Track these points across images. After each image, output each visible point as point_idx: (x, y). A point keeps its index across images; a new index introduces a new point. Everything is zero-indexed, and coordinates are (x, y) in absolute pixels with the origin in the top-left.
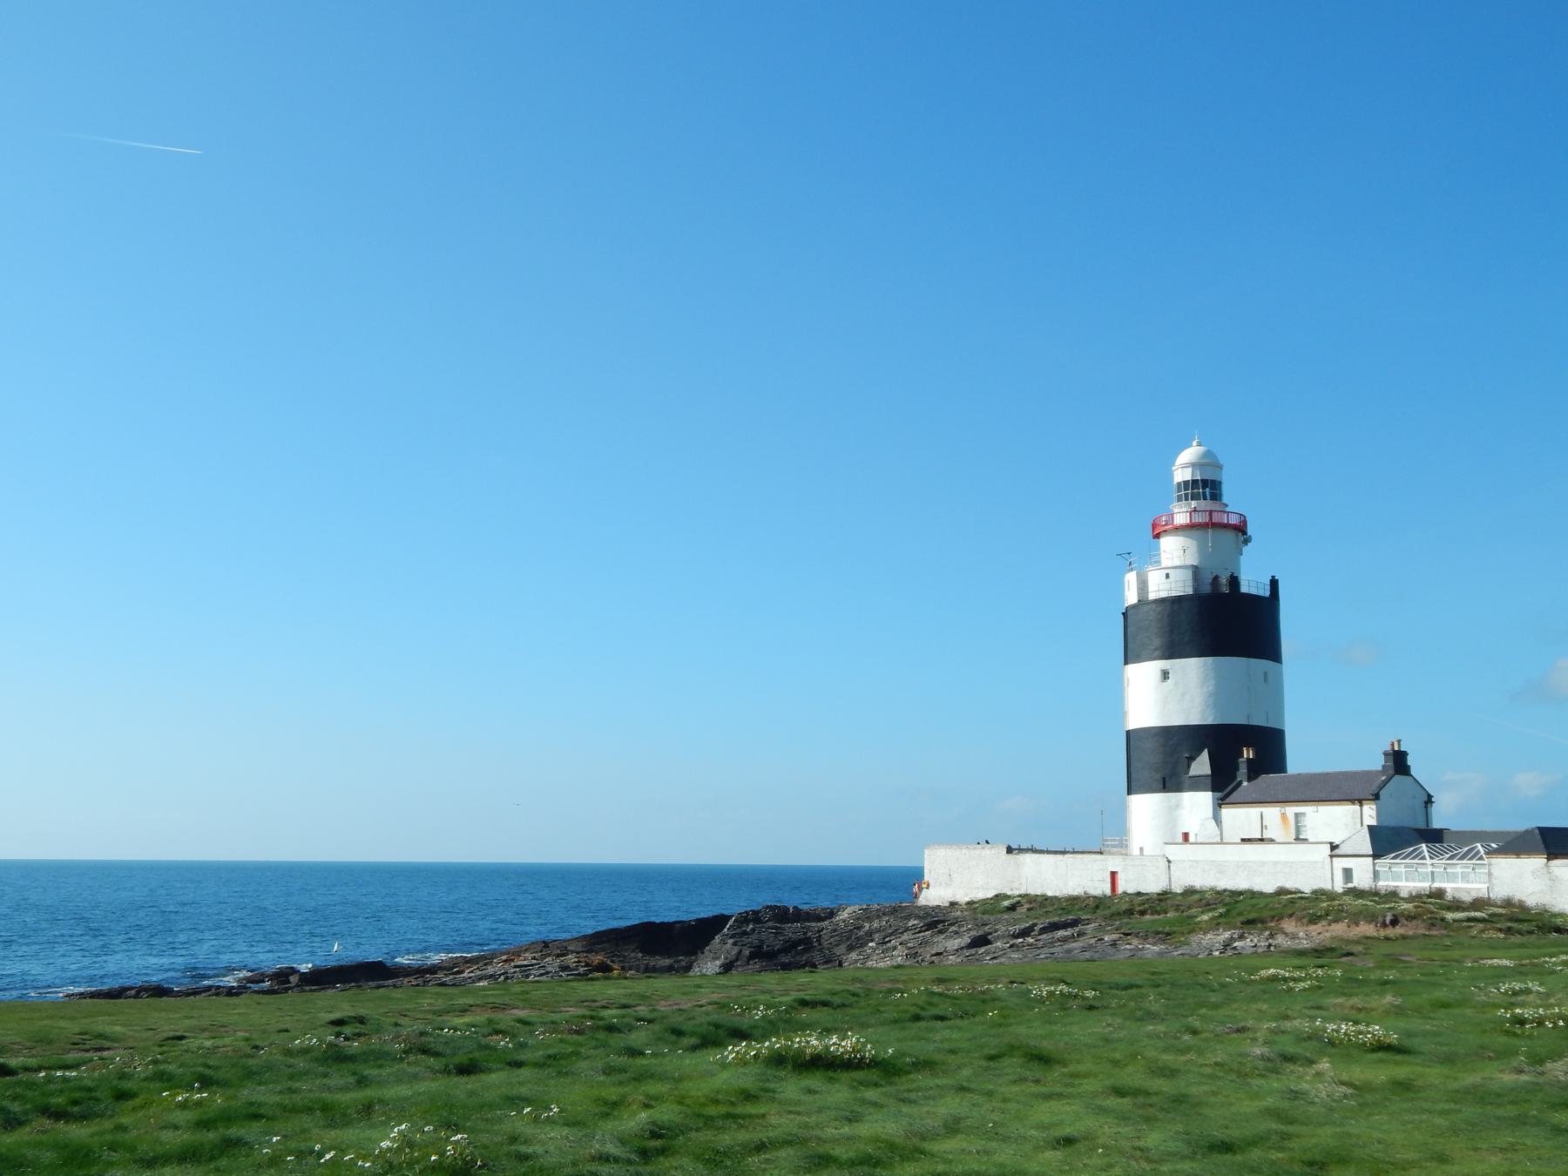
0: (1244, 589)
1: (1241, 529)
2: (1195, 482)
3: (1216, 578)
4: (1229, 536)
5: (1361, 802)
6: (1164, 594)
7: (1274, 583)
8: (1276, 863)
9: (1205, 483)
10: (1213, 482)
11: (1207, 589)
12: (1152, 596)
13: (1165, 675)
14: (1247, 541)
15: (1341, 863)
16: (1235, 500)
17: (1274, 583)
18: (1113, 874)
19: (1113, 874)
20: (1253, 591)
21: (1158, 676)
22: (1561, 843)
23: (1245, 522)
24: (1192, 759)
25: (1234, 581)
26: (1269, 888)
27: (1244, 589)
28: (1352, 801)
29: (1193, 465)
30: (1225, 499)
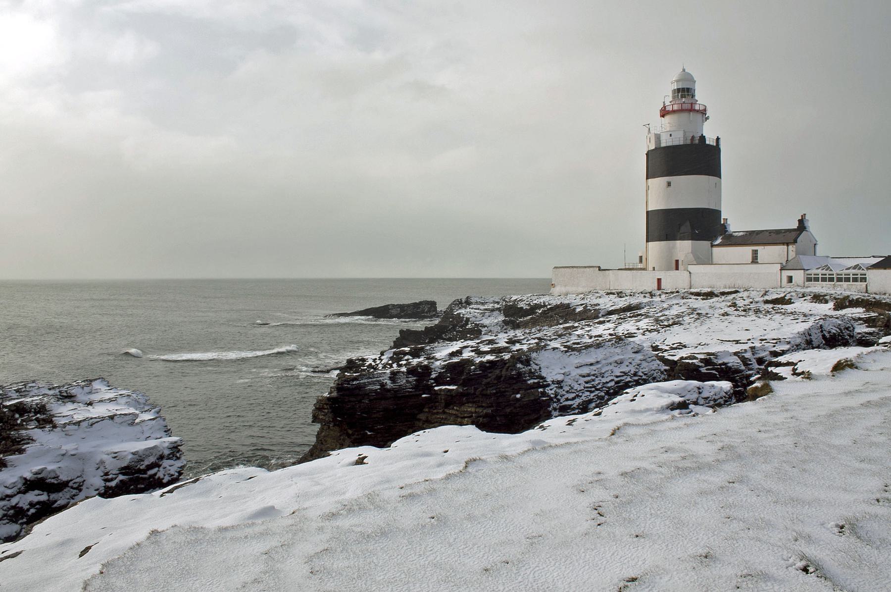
0: (707, 142)
1: (703, 112)
2: (678, 90)
3: (693, 137)
4: (700, 116)
5: (788, 244)
6: (670, 144)
7: (718, 139)
8: (283, 466)
9: (683, 90)
10: (688, 90)
11: (689, 142)
12: (663, 145)
13: (669, 184)
14: (707, 118)
15: (786, 273)
16: (701, 97)
17: (718, 139)
18: (659, 280)
19: (659, 280)
20: (711, 143)
21: (666, 184)
22: (890, 262)
23: (705, 110)
24: (680, 226)
25: (703, 138)
26: (393, 445)
27: (707, 142)
28: (783, 244)
29: (677, 81)
30: (696, 98)
